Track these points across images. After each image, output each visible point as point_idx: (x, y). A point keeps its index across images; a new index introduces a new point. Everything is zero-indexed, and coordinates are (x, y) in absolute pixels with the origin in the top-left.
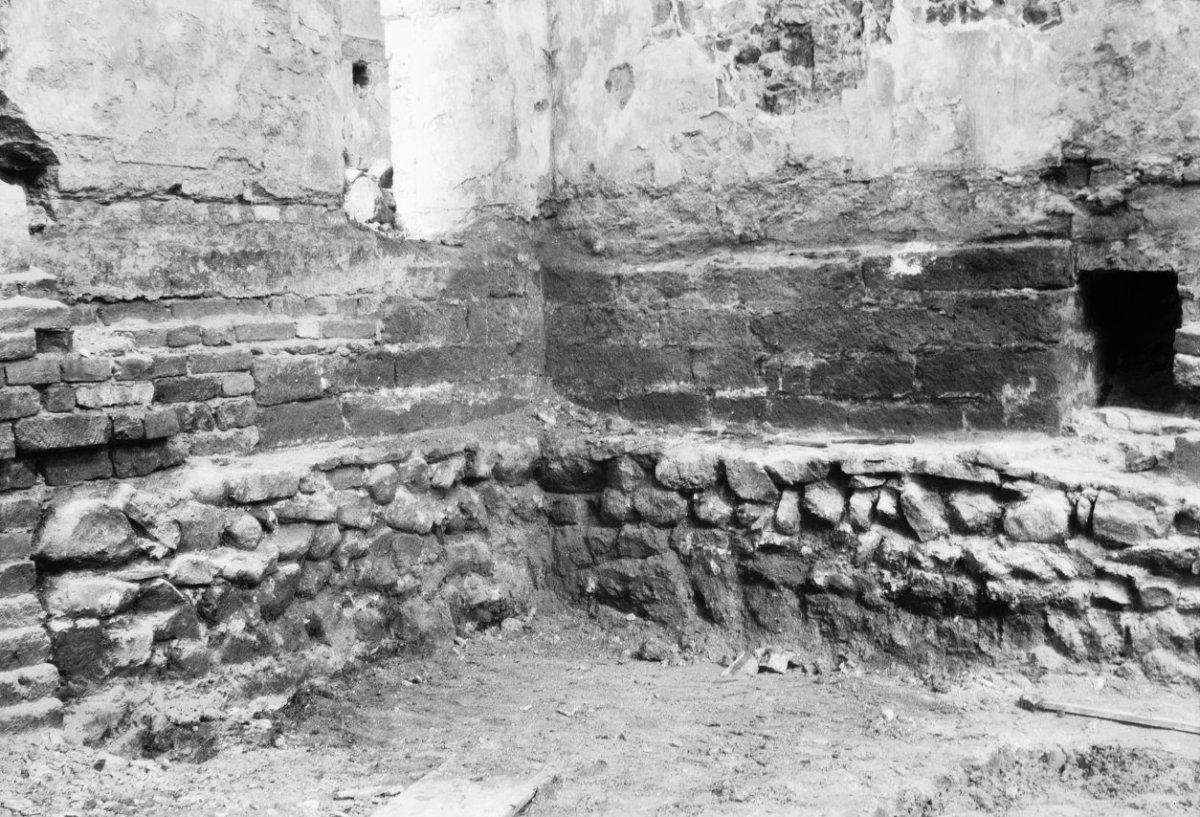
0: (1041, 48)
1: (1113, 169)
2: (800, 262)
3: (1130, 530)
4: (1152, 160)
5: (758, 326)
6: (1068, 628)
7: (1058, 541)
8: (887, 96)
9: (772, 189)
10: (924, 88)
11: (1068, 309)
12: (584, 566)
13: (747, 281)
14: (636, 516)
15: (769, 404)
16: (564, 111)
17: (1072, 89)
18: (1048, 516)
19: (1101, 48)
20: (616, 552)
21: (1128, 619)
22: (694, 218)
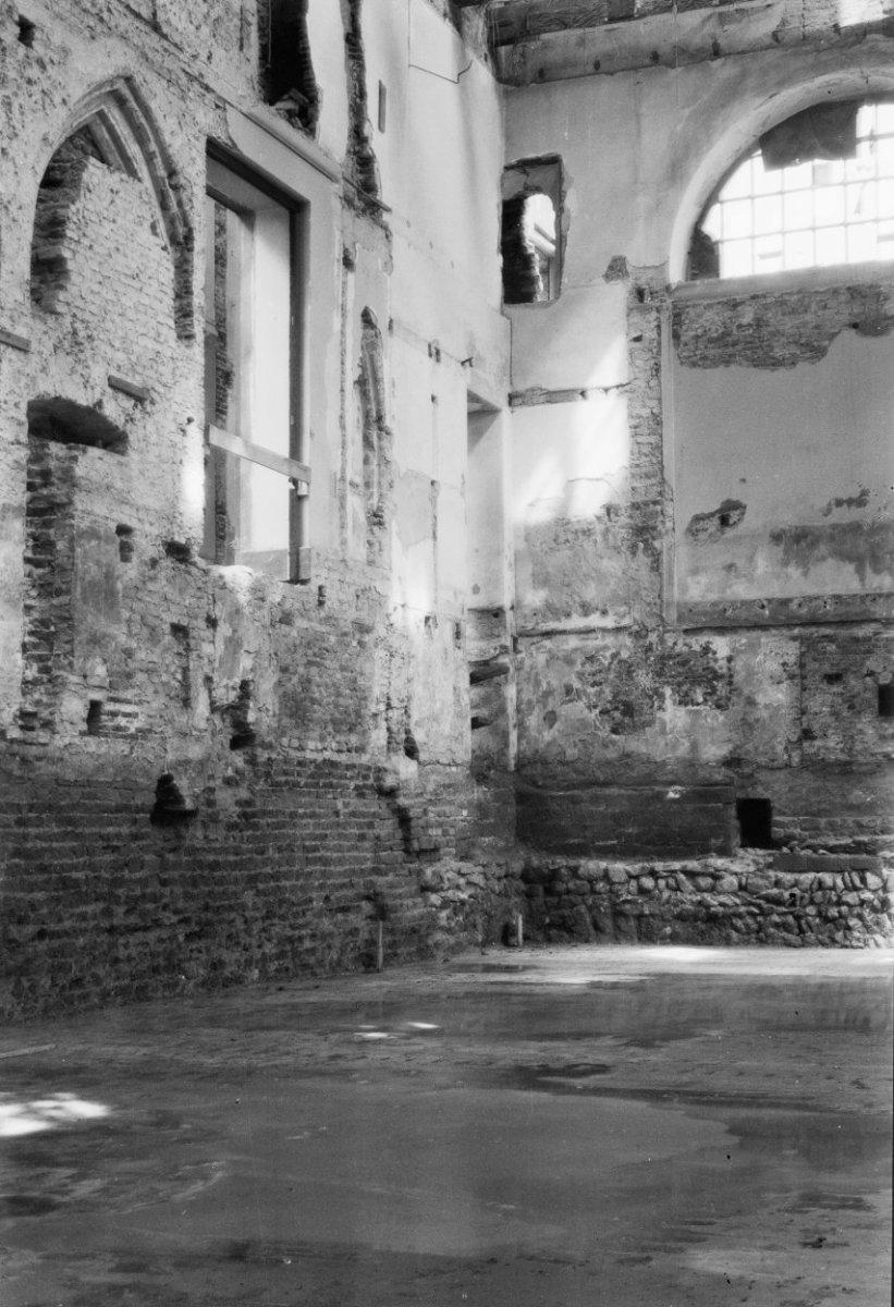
0: (721, 718)
1: (749, 763)
2: (630, 792)
3: (758, 887)
4: (762, 760)
5: (614, 817)
6: (739, 923)
7: (735, 894)
8: (663, 732)
9: (617, 763)
10: (678, 729)
11: (733, 812)
12: (544, 913)
13: (608, 800)
14: (568, 892)
15: (618, 847)
16: (524, 728)
17: (733, 734)
18: (732, 883)
19: (743, 719)
20: (558, 907)
21: (760, 919)
22: (583, 773)
